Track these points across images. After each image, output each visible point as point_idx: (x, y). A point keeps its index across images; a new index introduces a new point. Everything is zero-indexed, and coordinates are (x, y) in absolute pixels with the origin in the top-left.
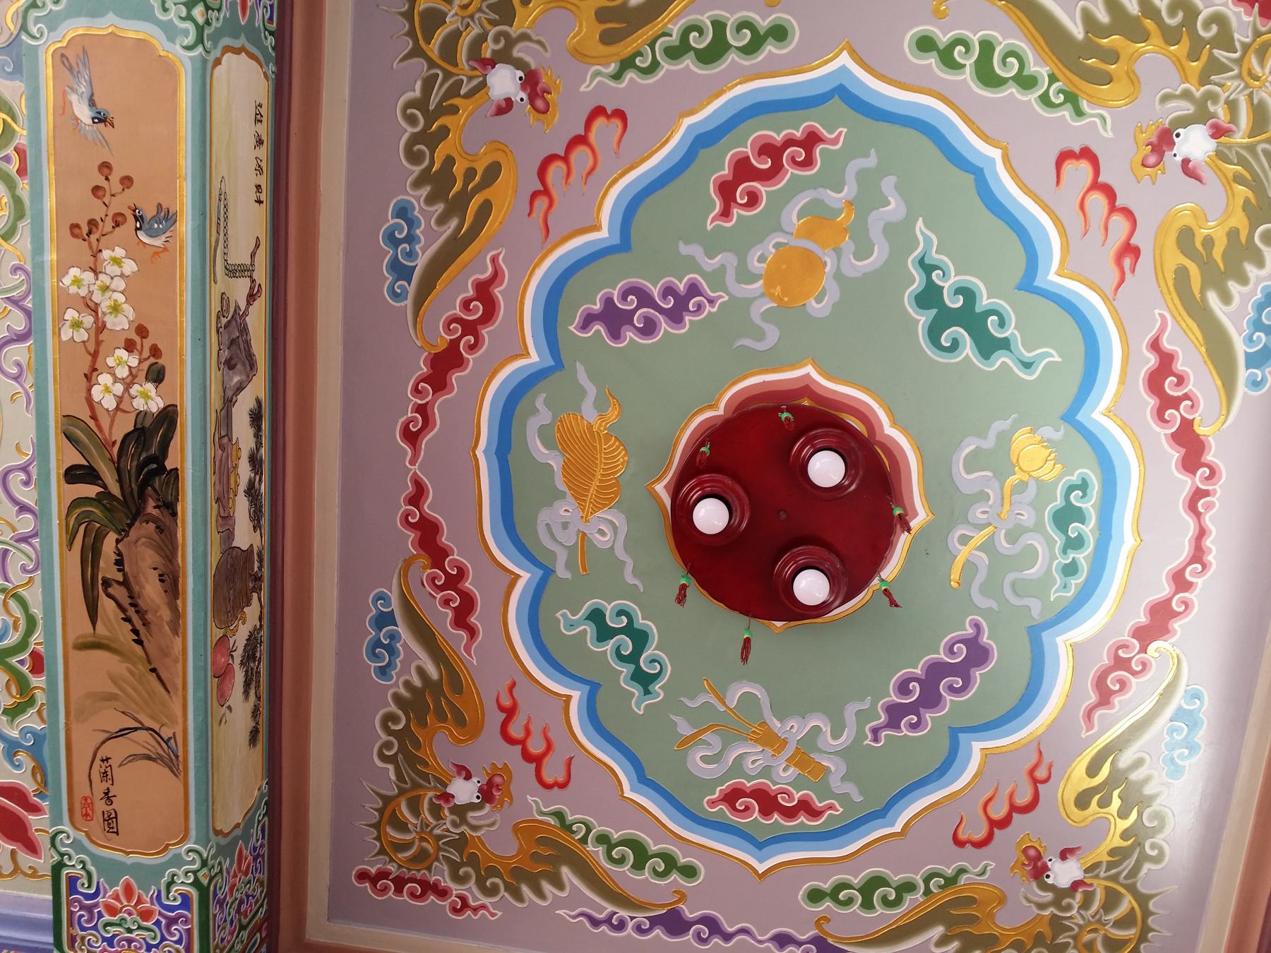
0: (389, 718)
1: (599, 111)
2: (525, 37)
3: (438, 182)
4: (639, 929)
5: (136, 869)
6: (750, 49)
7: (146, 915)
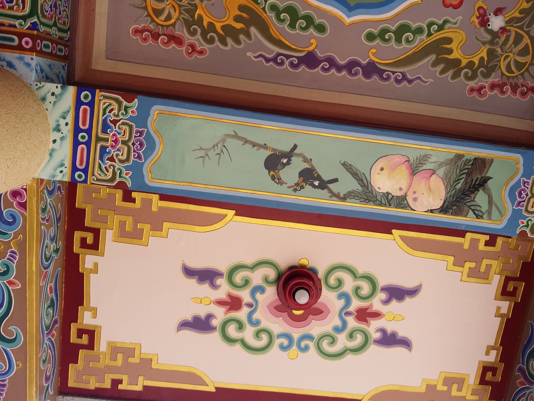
2: (484, 43)
4: (292, 65)
6: (384, 31)
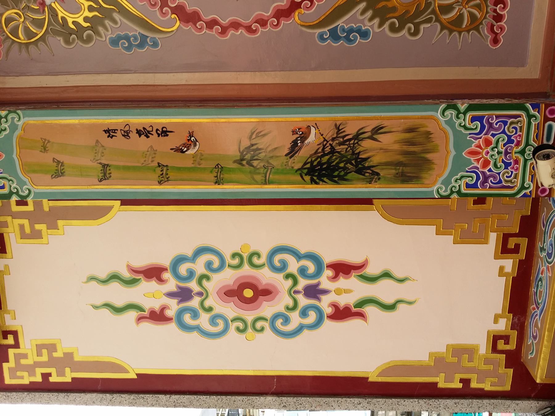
0: (393, 28)
5: (458, 147)
7: (488, 143)
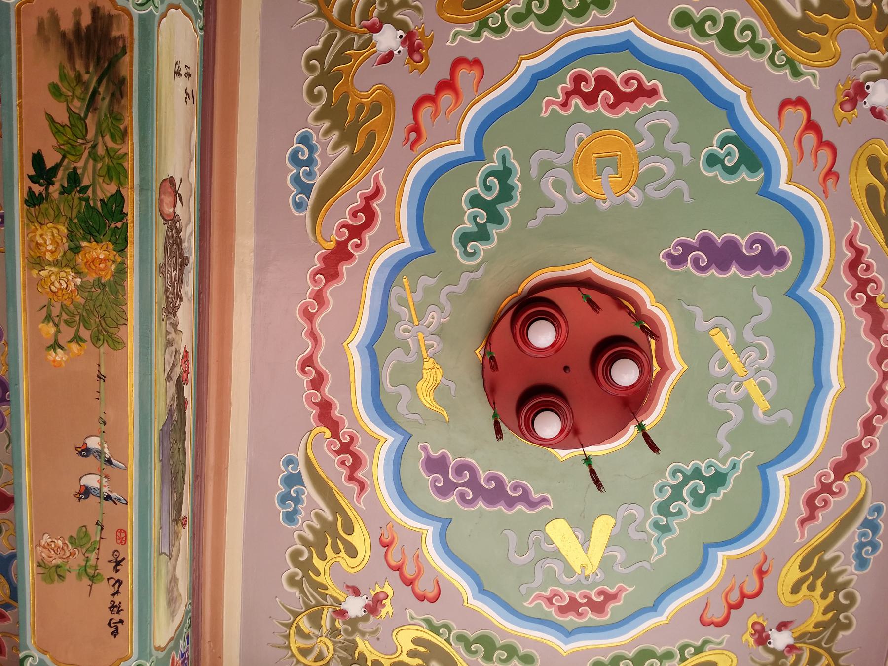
1: (458, 62)
3: (333, 114)
